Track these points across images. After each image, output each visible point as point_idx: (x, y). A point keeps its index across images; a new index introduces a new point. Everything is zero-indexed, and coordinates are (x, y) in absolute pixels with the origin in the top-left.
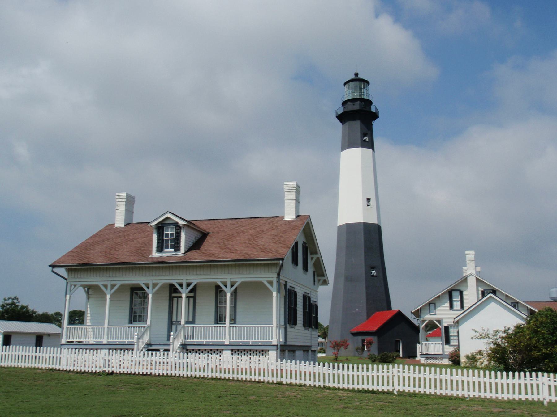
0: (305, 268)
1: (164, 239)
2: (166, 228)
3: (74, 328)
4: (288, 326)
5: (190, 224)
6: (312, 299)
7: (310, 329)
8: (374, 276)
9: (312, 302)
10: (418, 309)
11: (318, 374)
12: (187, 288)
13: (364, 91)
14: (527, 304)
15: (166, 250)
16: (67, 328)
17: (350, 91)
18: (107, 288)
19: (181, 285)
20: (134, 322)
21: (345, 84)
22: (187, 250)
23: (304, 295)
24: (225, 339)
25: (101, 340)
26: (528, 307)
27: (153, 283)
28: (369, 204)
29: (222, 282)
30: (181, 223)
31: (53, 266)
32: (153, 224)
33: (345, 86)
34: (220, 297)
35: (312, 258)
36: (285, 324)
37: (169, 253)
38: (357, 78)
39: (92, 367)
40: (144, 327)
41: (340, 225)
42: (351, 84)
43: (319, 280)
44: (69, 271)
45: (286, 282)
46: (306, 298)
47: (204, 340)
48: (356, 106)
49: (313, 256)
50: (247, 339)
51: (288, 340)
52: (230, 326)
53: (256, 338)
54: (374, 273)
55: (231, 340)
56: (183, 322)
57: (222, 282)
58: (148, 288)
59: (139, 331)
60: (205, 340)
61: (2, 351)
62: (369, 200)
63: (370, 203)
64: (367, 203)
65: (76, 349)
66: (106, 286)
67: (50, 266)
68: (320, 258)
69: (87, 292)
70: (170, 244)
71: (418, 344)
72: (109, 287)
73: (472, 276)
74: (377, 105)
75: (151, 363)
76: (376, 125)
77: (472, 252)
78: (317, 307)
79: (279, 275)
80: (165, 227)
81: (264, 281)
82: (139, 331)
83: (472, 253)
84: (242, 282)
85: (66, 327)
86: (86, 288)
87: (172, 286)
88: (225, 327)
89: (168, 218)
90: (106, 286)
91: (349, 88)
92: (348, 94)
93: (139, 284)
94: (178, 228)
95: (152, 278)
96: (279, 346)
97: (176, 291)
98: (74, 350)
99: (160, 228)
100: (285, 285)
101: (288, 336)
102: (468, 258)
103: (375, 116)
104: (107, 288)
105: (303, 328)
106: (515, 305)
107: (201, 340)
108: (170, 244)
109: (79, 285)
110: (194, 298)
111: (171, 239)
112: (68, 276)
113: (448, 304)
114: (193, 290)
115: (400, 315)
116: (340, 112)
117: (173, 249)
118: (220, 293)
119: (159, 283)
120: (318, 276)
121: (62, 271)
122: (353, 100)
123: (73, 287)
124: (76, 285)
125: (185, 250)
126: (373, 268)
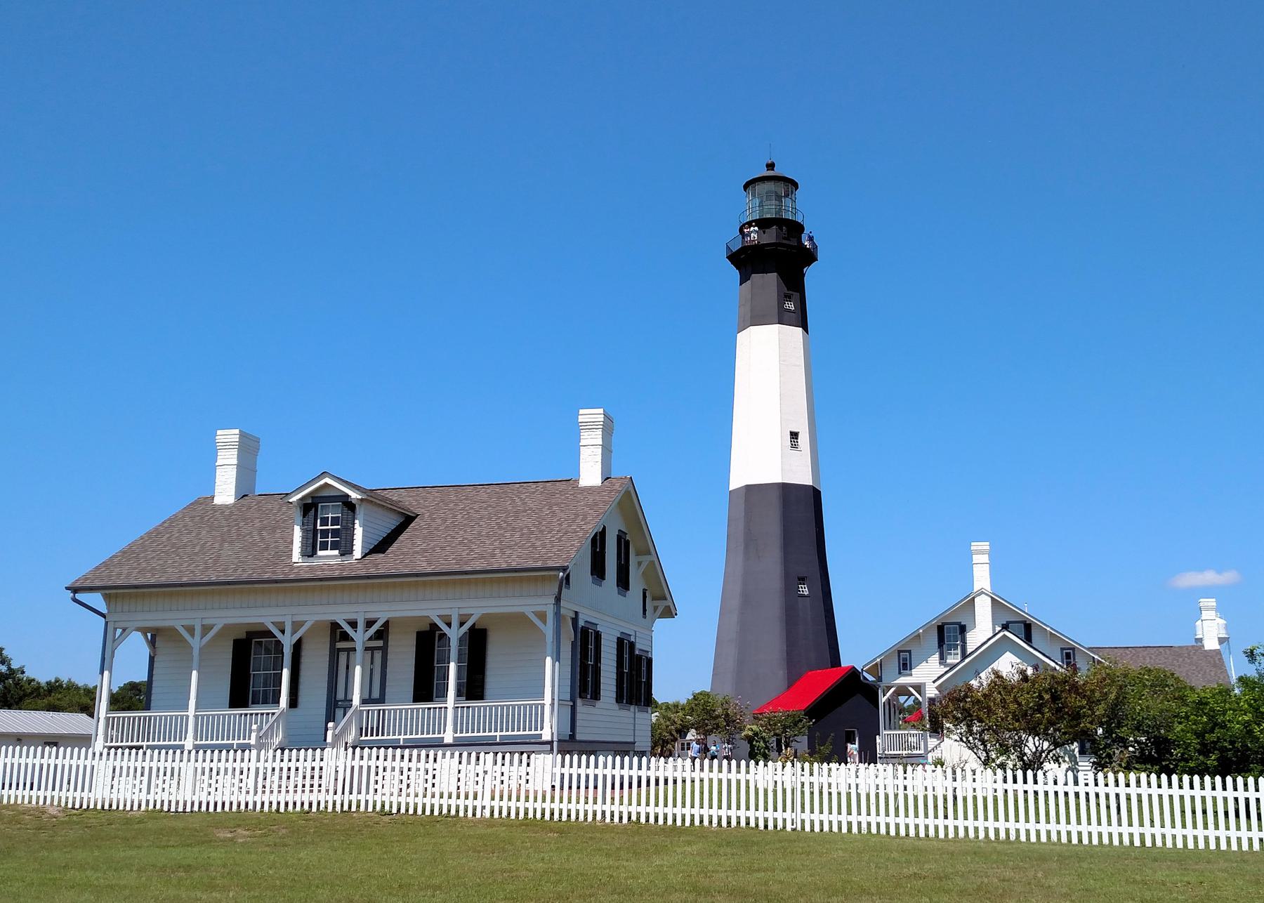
0: (623, 582)
1: (317, 530)
2: (322, 506)
3: (132, 719)
4: (579, 701)
5: (374, 498)
6: (638, 646)
7: (632, 708)
8: (803, 596)
9: (637, 652)
10: (876, 664)
11: (160, 803)
12: (367, 631)
13: (787, 202)
14: (1092, 652)
15: (320, 553)
16: (107, 719)
17: (757, 201)
18: (193, 635)
19: (353, 624)
20: (252, 703)
21: (746, 187)
22: (364, 554)
23: (618, 638)
24: (541, 730)
25: (180, 743)
26: (1094, 658)
27: (293, 622)
28: (795, 445)
29: (536, 613)
30: (354, 495)
31: (75, 590)
32: (294, 499)
33: (745, 190)
34: (438, 647)
35: (640, 564)
36: (573, 700)
37: (328, 556)
38: (771, 173)
39: (392, 795)
40: (273, 714)
41: (734, 488)
42: (760, 188)
43: (656, 608)
44: (107, 598)
45: (576, 613)
46: (624, 645)
47: (399, 737)
48: (770, 237)
49: (641, 558)
50: (228, 739)
51: (578, 730)
52: (456, 705)
53: (229, 737)
54: (804, 590)
55: (458, 735)
56: (356, 700)
57: (536, 613)
58: (283, 632)
59: (262, 723)
60: (498, 734)
61: (1258, 800)
62: (794, 435)
63: (797, 442)
64: (791, 441)
65: (522, 753)
66: (191, 630)
67: (67, 588)
68: (657, 563)
69: (152, 643)
70: (330, 539)
71: (877, 737)
72: (455, 624)
73: (983, 595)
74: (816, 229)
75: (287, 787)
76: (811, 274)
77: (985, 546)
78: (650, 662)
79: (558, 599)
80: (320, 505)
81: (528, 611)
82: (262, 723)
83: (985, 548)
84: (317, 621)
85: (104, 716)
86: (149, 635)
87: (335, 626)
88: (446, 708)
89: (326, 485)
90: (191, 630)
91: (754, 196)
92: (750, 207)
93: (523, 613)
94: (349, 506)
95: (459, 604)
96: (555, 744)
97: (345, 637)
98: (517, 756)
99: (310, 507)
100: (575, 620)
101: (578, 723)
102: (976, 558)
103: (809, 257)
104: (193, 635)
105: (616, 706)
106: (1070, 653)
107: (228, 742)
108: (330, 539)
109: (133, 628)
110: (384, 650)
111: (332, 529)
112: (108, 609)
113: (937, 656)
114: (382, 634)
115: (853, 673)
116: (736, 247)
117: (338, 551)
118: (439, 640)
119: (214, 625)
120: (654, 599)
121: (96, 600)
122: (763, 224)
123: (119, 631)
124: (127, 628)
125: (362, 552)
126: (802, 580)
